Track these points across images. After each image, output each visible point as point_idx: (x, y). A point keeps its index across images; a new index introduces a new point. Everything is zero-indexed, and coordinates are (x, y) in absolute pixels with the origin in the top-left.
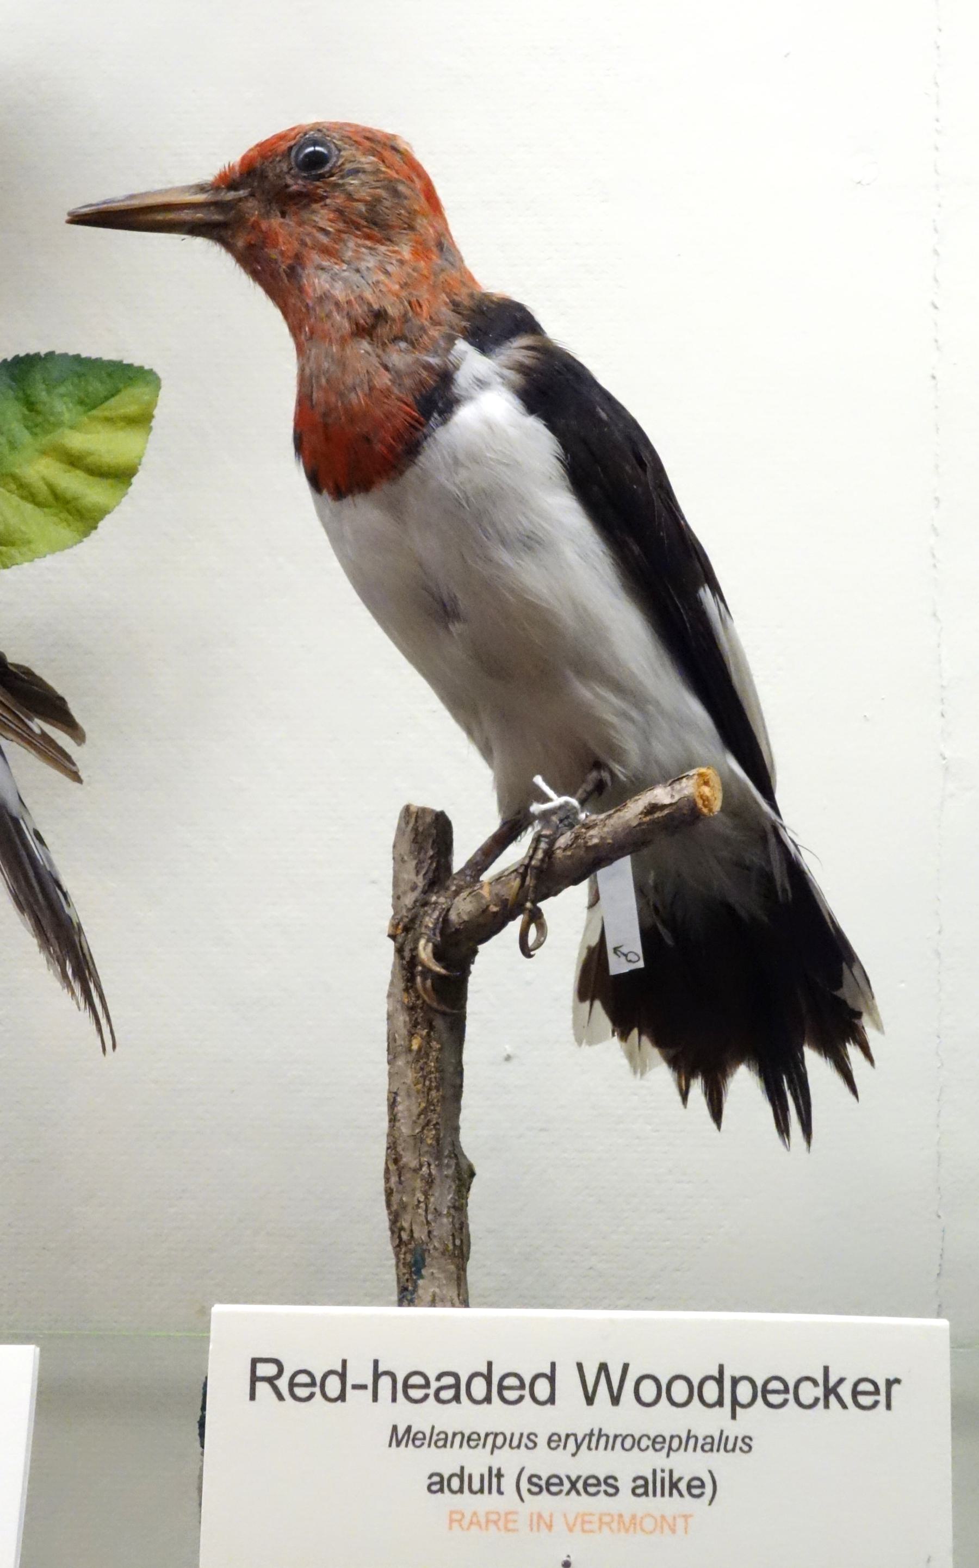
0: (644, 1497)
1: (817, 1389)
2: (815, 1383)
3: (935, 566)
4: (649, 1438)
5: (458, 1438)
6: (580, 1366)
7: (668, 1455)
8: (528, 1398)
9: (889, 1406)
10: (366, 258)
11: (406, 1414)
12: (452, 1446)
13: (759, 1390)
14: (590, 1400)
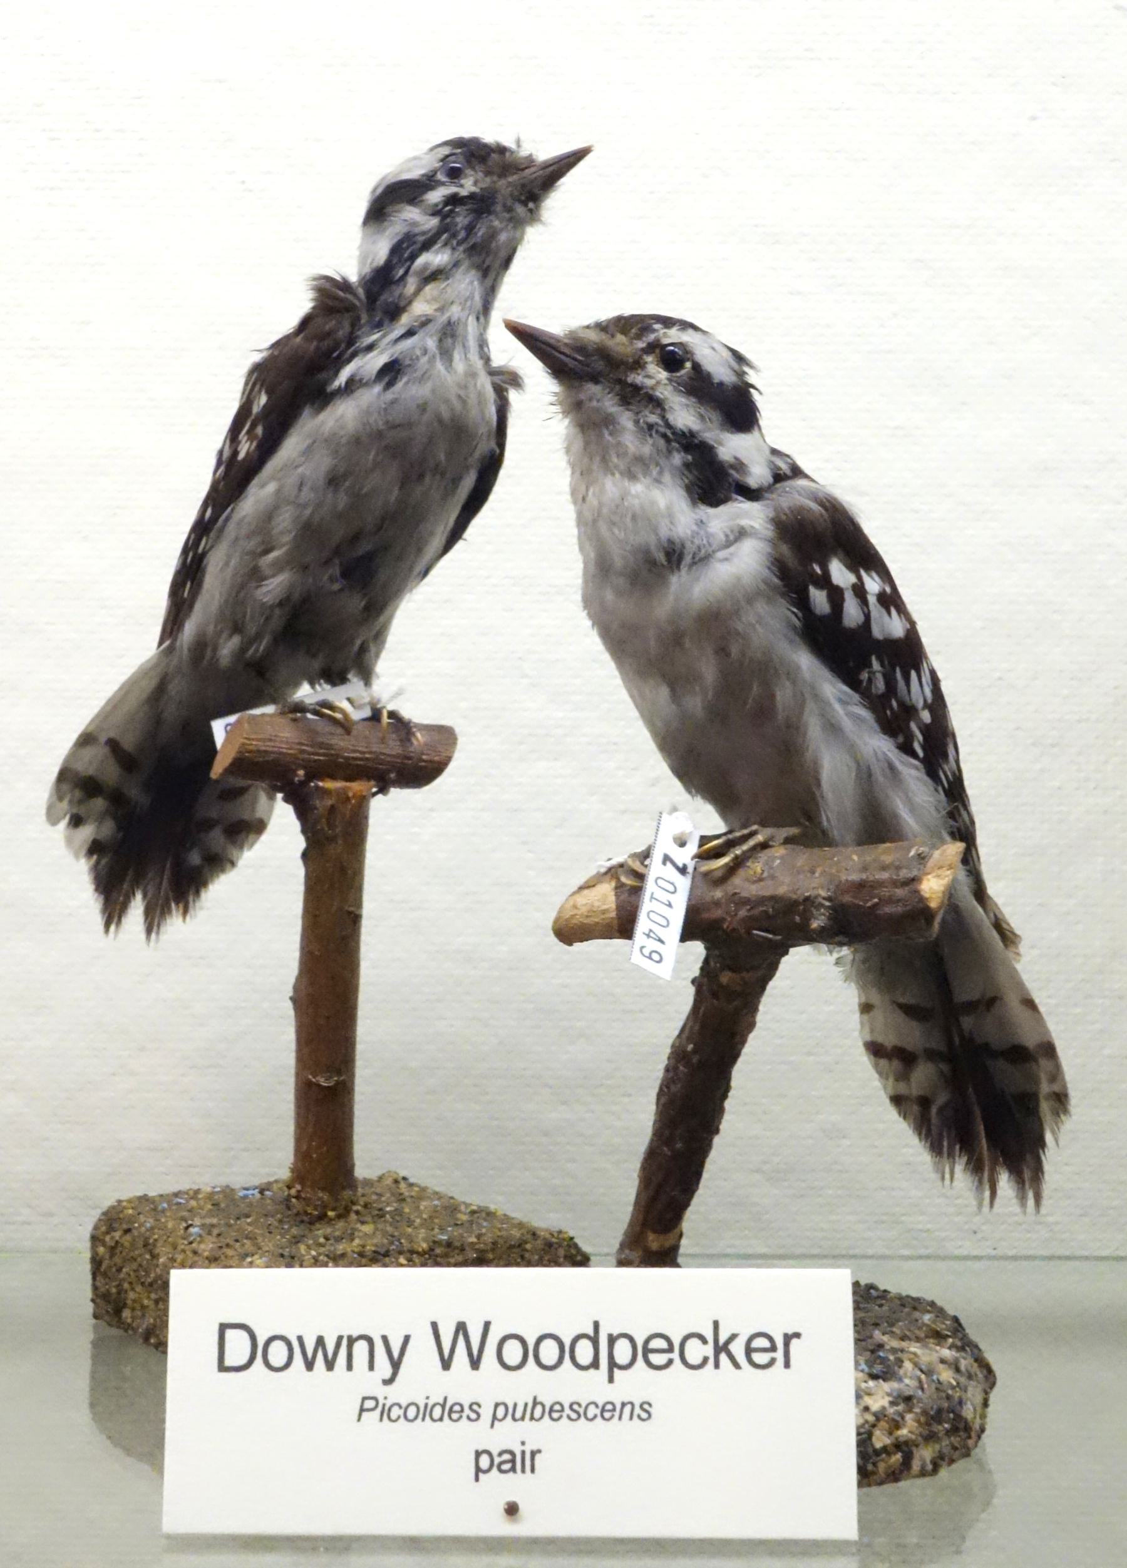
0: (511, 1474)
1: (705, 1347)
2: (704, 1341)
4: (400, 1407)
5: (518, 1415)
6: (434, 1326)
9: (787, 1365)
13: (567, 1349)
14: (446, 1364)
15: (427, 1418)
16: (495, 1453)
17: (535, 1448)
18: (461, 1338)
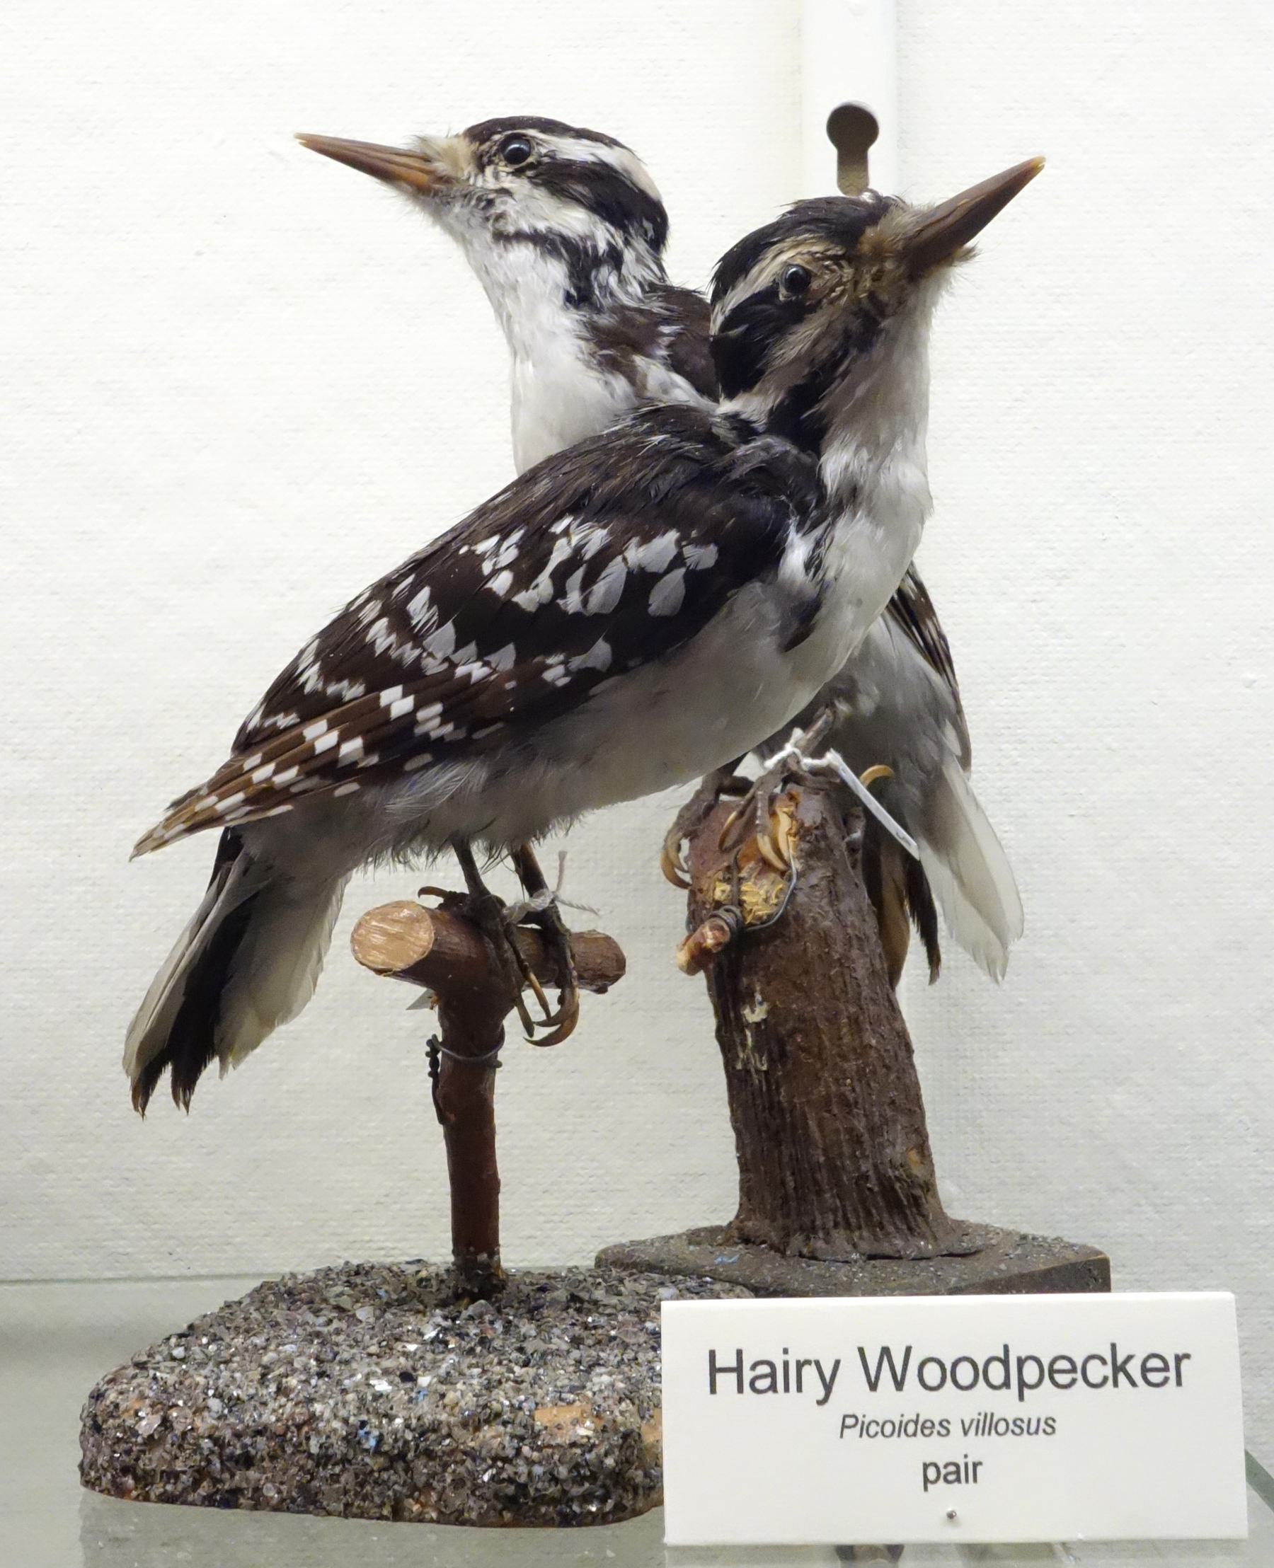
0: (956, 1484)
4: (877, 1424)
6: (861, 1351)
8: (1080, 1382)
9: (1179, 1383)
14: (873, 1386)
15: (993, 1431)
16: (941, 1465)
17: (976, 1460)
18: (885, 1364)
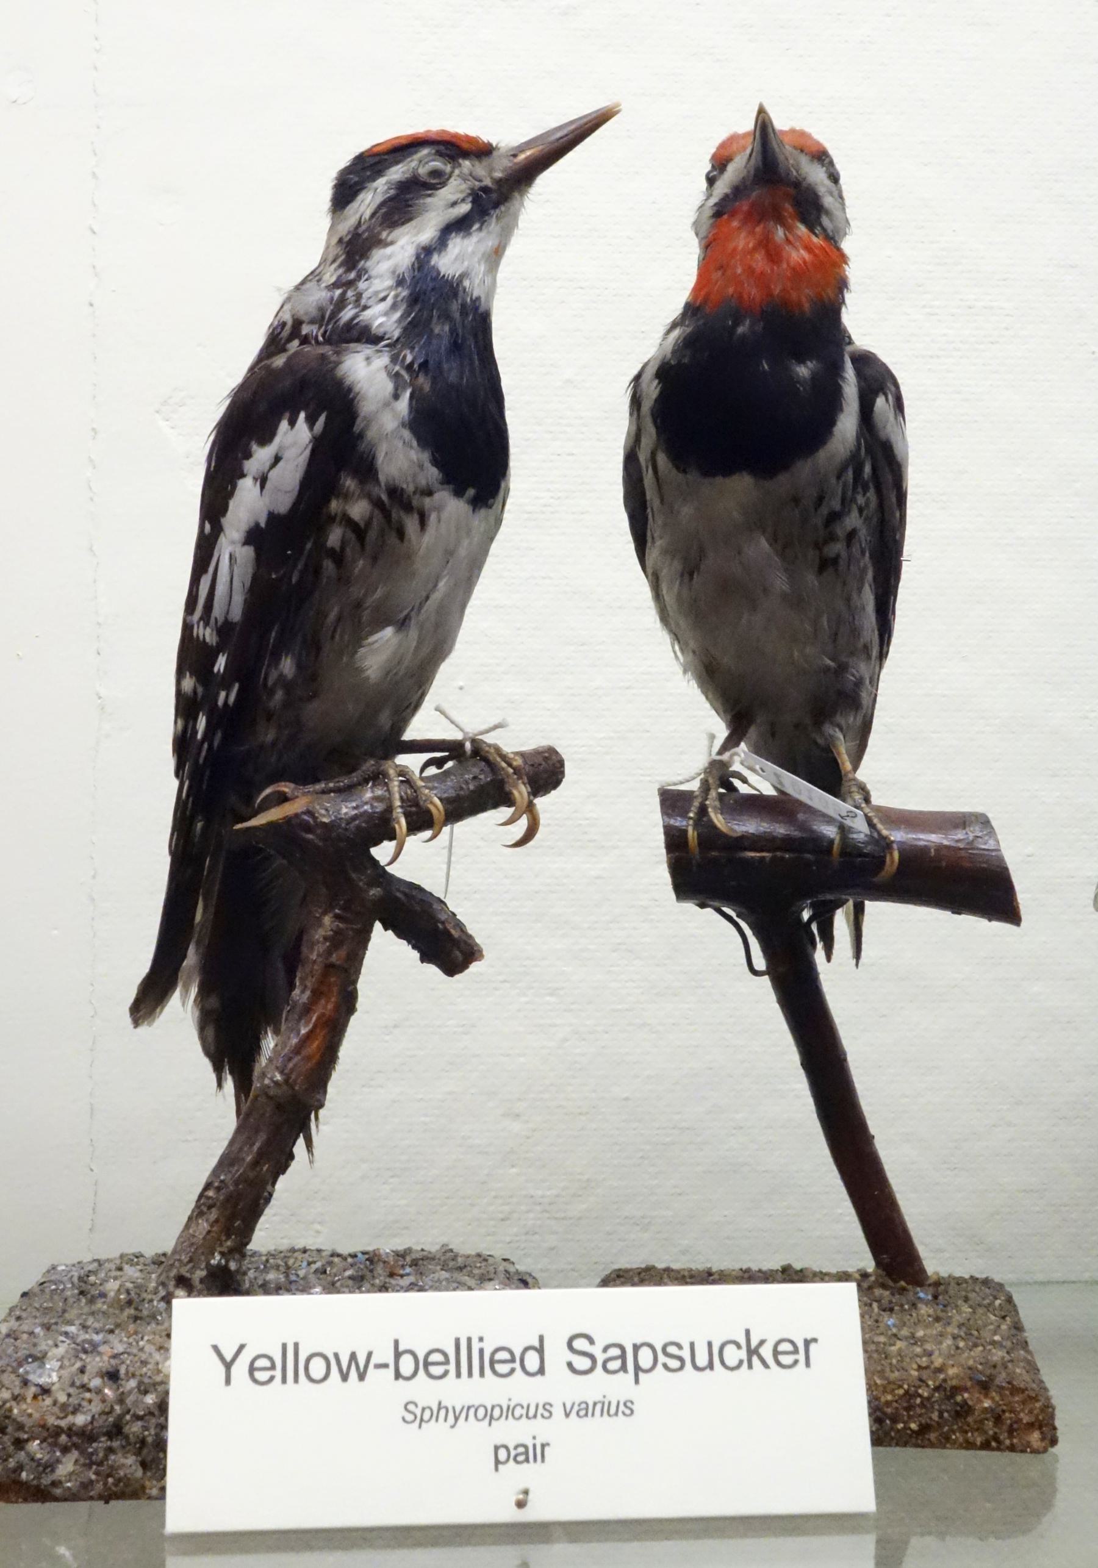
0: (525, 1465)
3: (92, 499)
7: (420, 1427)
9: (808, 1364)
10: (341, 271)
11: (424, 1391)
12: (593, 1415)
16: (511, 1448)
